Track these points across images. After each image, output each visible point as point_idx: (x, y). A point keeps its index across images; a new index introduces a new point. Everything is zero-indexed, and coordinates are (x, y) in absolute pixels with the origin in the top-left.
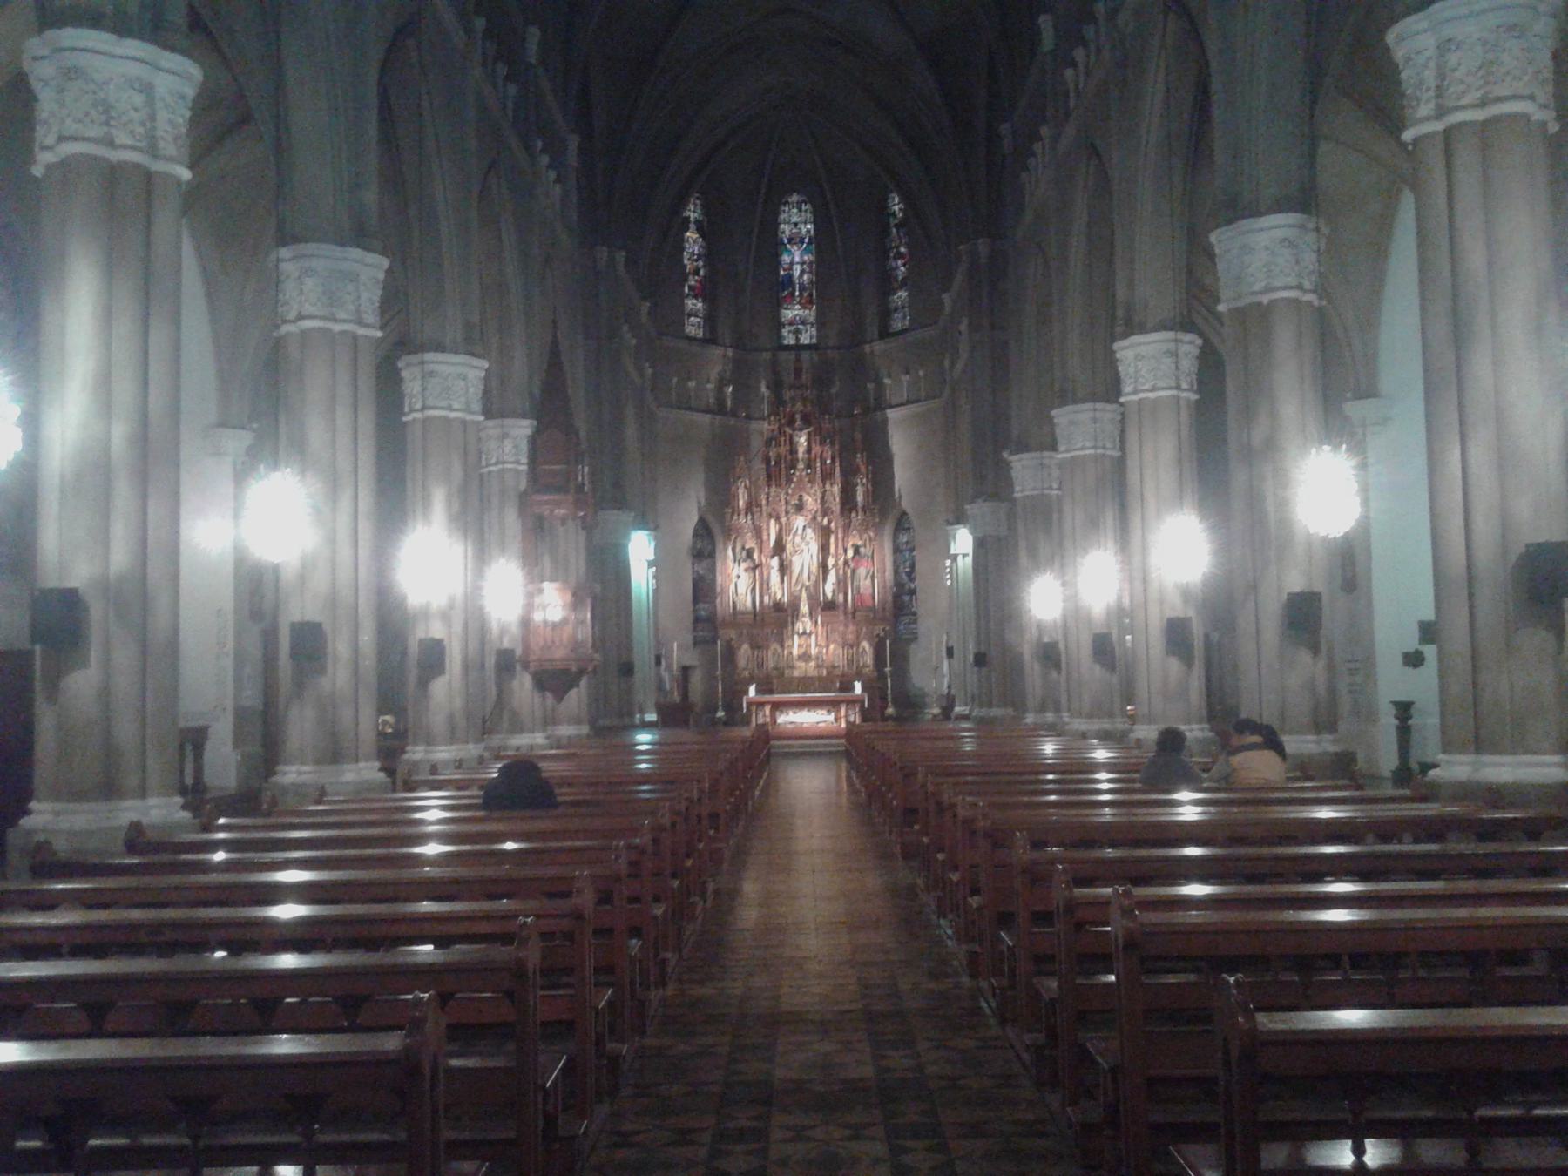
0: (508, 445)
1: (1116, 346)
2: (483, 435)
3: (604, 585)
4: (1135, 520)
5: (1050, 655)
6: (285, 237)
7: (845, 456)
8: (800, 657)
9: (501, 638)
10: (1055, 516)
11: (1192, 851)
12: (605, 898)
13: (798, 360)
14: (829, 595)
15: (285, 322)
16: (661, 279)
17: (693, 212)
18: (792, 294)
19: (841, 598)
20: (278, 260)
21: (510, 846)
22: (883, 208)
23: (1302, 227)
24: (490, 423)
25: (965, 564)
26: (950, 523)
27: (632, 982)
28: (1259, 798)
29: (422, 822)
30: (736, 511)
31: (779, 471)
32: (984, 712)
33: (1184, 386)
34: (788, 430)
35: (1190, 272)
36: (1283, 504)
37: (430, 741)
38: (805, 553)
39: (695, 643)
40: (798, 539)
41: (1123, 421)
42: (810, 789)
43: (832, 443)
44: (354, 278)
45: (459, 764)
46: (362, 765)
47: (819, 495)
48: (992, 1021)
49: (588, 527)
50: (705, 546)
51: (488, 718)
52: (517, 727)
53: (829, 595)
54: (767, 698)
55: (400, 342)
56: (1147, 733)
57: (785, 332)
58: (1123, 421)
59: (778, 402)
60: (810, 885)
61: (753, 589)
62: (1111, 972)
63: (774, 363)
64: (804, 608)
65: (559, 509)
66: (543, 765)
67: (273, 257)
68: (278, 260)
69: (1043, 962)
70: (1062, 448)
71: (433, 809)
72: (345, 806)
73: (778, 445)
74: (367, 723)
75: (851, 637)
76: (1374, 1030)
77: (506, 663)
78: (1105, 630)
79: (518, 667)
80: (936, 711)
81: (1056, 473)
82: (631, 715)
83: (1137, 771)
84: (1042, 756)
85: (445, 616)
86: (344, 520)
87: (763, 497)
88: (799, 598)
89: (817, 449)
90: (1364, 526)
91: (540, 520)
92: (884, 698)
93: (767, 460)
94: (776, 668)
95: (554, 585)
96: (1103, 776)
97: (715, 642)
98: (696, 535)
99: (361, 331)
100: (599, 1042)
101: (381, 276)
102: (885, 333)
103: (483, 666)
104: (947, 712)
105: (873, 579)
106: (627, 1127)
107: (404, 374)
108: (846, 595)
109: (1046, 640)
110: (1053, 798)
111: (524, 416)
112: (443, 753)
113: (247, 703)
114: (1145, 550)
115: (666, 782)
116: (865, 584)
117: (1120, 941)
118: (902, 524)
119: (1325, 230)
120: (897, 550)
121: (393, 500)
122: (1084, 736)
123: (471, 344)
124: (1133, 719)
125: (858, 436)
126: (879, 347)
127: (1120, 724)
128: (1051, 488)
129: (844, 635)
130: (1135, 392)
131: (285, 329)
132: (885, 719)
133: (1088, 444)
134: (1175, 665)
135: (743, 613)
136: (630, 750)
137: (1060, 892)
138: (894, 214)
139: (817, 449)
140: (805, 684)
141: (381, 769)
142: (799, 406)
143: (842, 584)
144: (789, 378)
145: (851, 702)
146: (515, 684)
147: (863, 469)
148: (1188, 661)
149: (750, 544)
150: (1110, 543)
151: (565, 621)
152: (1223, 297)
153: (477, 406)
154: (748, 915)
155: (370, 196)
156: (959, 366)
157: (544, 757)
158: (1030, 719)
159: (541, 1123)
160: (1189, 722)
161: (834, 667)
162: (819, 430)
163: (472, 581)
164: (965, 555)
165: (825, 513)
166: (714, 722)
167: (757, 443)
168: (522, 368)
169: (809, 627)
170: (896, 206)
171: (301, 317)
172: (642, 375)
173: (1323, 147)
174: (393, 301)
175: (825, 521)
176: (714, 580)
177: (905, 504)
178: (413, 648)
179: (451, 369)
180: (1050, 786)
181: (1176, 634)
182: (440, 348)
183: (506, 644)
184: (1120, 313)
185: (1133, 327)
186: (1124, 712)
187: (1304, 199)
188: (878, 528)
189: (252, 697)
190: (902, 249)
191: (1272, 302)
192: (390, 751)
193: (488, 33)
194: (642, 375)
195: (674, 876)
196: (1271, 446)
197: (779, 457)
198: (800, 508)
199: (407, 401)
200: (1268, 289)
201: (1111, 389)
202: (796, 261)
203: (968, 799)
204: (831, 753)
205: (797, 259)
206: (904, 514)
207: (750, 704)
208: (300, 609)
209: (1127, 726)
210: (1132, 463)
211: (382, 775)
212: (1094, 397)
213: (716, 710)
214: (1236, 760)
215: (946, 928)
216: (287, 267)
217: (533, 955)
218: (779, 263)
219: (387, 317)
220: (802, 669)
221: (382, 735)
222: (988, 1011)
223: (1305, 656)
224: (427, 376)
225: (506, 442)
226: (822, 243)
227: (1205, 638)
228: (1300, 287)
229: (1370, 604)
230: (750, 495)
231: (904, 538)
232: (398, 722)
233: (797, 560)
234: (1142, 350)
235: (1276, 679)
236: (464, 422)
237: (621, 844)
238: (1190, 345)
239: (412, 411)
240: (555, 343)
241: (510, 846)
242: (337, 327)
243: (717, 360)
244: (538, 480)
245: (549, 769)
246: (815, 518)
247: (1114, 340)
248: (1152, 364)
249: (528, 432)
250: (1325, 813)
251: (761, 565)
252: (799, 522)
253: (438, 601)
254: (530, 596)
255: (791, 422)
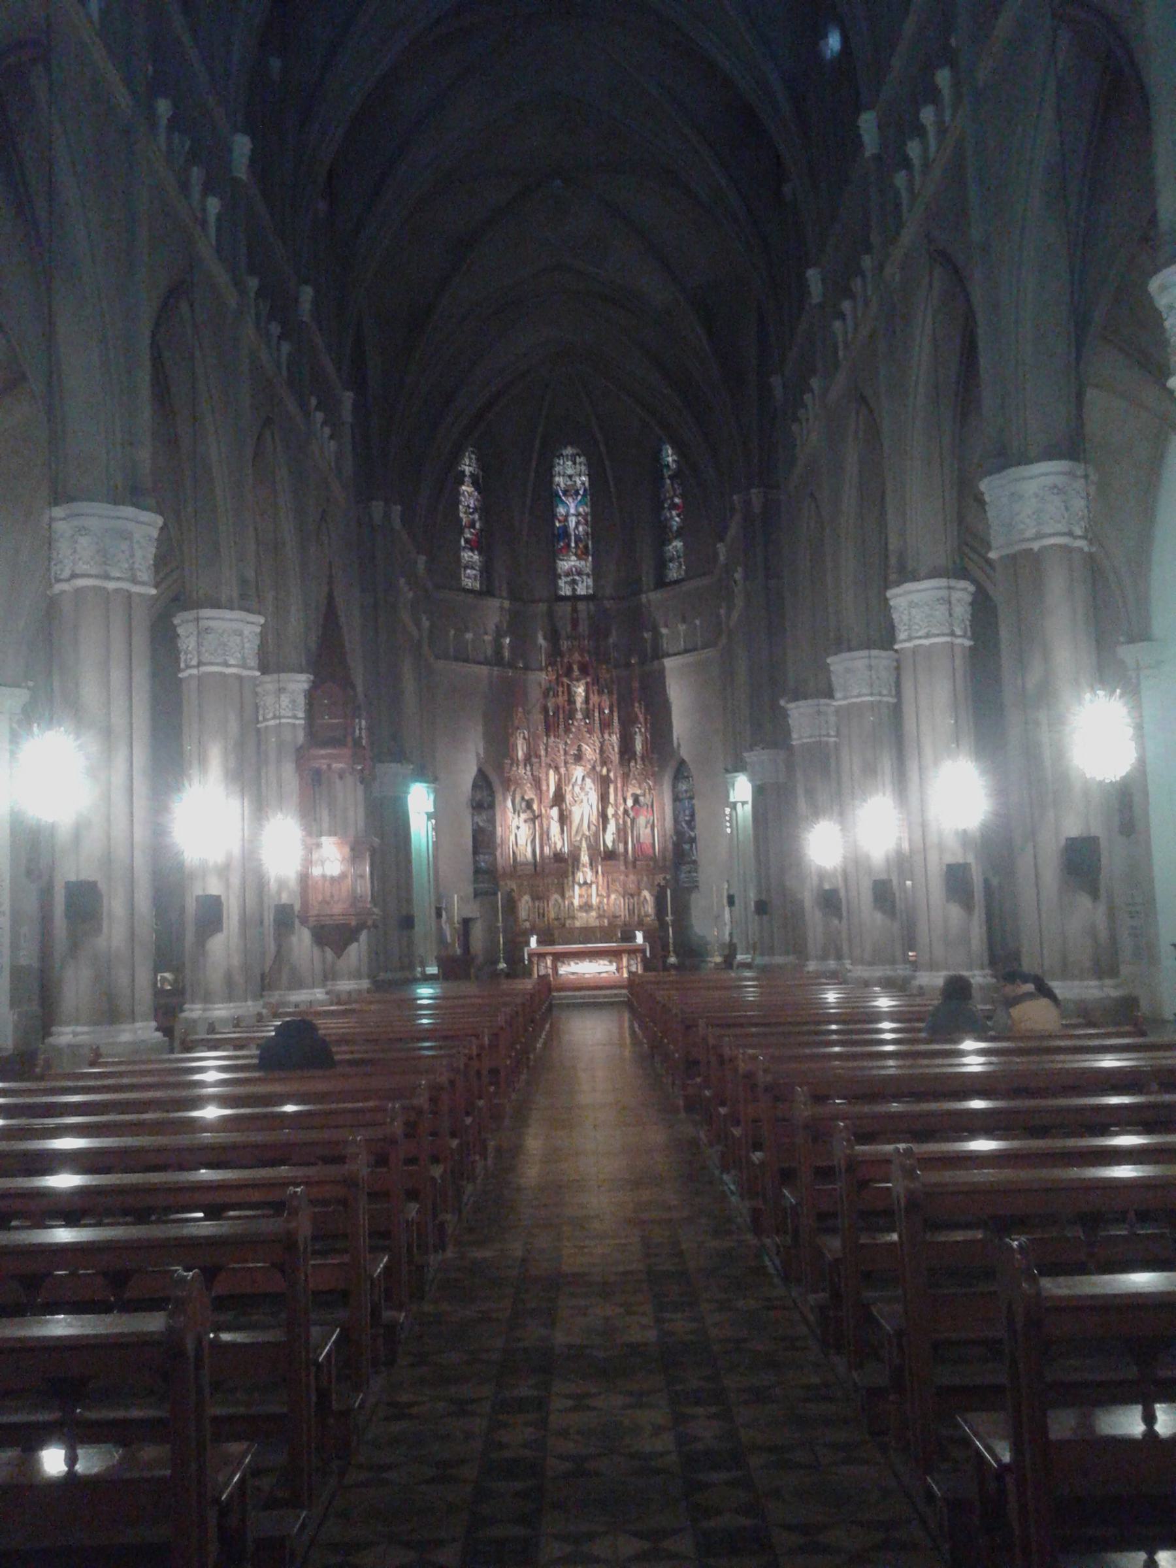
0: (285, 700)
1: (889, 594)
2: (259, 689)
3: (384, 840)
4: (913, 775)
5: (830, 901)
6: (59, 496)
7: (623, 704)
8: (581, 907)
9: (279, 893)
10: (833, 762)
11: (977, 1104)
12: (381, 1160)
13: (575, 610)
14: (610, 845)
15: (58, 581)
16: (438, 530)
17: (468, 466)
18: (568, 545)
19: (621, 847)
20: (51, 519)
21: (290, 1108)
22: (657, 456)
23: (1071, 474)
24: (267, 678)
25: (745, 812)
26: (727, 771)
27: (410, 1247)
28: (1039, 1046)
29: (202, 1084)
30: (515, 762)
31: (557, 721)
32: (766, 960)
33: (959, 632)
34: (565, 680)
35: (961, 519)
36: (1060, 755)
37: (207, 998)
38: (584, 803)
39: (476, 895)
40: (577, 789)
41: (898, 668)
42: (593, 1038)
43: (610, 693)
44: (127, 536)
45: (237, 1022)
46: (138, 1025)
47: (598, 744)
48: (776, 1280)
49: (366, 780)
50: (484, 799)
51: (265, 978)
52: (297, 983)
53: (610, 845)
54: (550, 949)
55: (177, 594)
56: (934, 980)
57: (561, 583)
58: (898, 668)
59: (555, 652)
60: (595, 1136)
61: (533, 840)
62: (894, 1231)
63: (550, 614)
64: (585, 858)
65: (335, 761)
66: (318, 1022)
67: (46, 519)
68: (51, 519)
69: (825, 1220)
70: (838, 695)
71: (211, 1069)
72: (123, 1068)
73: (556, 695)
74: (140, 981)
75: (632, 886)
76: (1162, 1294)
77: (285, 919)
78: (884, 876)
79: (297, 922)
80: (718, 959)
81: (833, 719)
82: (411, 967)
83: (919, 1020)
84: (825, 1005)
85: (224, 871)
86: (118, 779)
87: (542, 747)
88: (579, 849)
89: (594, 699)
90: (1142, 762)
91: (318, 773)
92: (665, 947)
93: (545, 710)
94: (557, 919)
95: (333, 839)
96: (886, 1025)
97: (495, 894)
98: (475, 786)
99: (136, 589)
100: (375, 1313)
101: (155, 534)
102: (661, 583)
103: (262, 923)
104: (729, 962)
105: (653, 828)
106: (404, 1398)
107: (180, 631)
108: (626, 844)
109: (827, 887)
110: (837, 1049)
111: (301, 671)
112: (221, 1011)
113: (24, 962)
114: (922, 802)
115: (446, 1038)
116: (644, 833)
117: (903, 1201)
118: (681, 772)
119: (1094, 477)
120: (676, 799)
121: (168, 760)
122: (867, 984)
123: (246, 601)
124: (915, 966)
125: (636, 685)
126: (655, 596)
127: (901, 971)
128: (828, 735)
129: (624, 885)
130: (910, 639)
131: (58, 587)
132: (666, 968)
133: (865, 691)
134: (955, 911)
135: (523, 864)
136: (411, 1003)
137: (841, 1149)
138: (668, 466)
139: (594, 699)
140: (587, 934)
141: (157, 1029)
142: (576, 656)
143: (622, 833)
144: (565, 628)
145: (631, 952)
146: (294, 939)
147: (641, 718)
148: (968, 907)
149: (530, 795)
150: (889, 788)
151: (343, 876)
152: (994, 544)
153: (253, 662)
154: (531, 1173)
155: (144, 454)
156: (735, 615)
157: (318, 1014)
158: (812, 966)
159: (314, 1399)
160: (970, 968)
161: (615, 917)
162: (596, 681)
163: (248, 837)
164: (744, 803)
165: (604, 763)
166: (496, 975)
167: (535, 694)
168: (298, 624)
169: (590, 876)
170: (670, 457)
171: (74, 576)
172: (418, 624)
173: (1091, 394)
174: (167, 559)
175: (604, 771)
176: (493, 833)
177: (684, 753)
178: (191, 906)
179: (227, 625)
180: (835, 1037)
181: (957, 880)
182: (217, 605)
183: (285, 898)
184: (893, 561)
185: (907, 575)
186: (906, 960)
187: (1072, 446)
188: (657, 777)
189: (28, 957)
190: (677, 500)
191: (1044, 549)
192: (167, 1010)
193: (259, 293)
194: (418, 624)
195: (453, 1135)
196: (1045, 695)
197: (557, 709)
198: (579, 758)
199: (183, 657)
200: (1039, 536)
201: (885, 637)
202: (572, 512)
203: (750, 1051)
204: (612, 1004)
205: (572, 511)
206: (682, 762)
207: (530, 956)
208: (70, 871)
209: (908, 973)
210: (908, 709)
211: (159, 1034)
212: (869, 645)
213: (497, 962)
214: (1015, 1012)
215: (729, 1181)
216: (61, 527)
217: (303, 1226)
218: (554, 516)
219: (162, 575)
220: (585, 919)
221: (158, 993)
222: (772, 1271)
223: (1084, 901)
224: (202, 632)
225: (283, 697)
226: (597, 494)
227: (987, 881)
228: (1070, 534)
229: (1148, 842)
230: (529, 747)
231: (683, 787)
232: (176, 981)
233: (576, 809)
234: (915, 597)
235: (1056, 922)
236: (239, 678)
237: (404, 1089)
238: (963, 591)
239: (188, 667)
240: (330, 597)
241: (290, 1108)
242: (111, 585)
243: (494, 611)
244: (316, 736)
245: (328, 1027)
246: (594, 768)
247: (886, 588)
248: (925, 610)
249: (306, 686)
250: (1109, 1062)
251: (540, 816)
252: (578, 772)
253: (216, 857)
254: (309, 850)
255: (569, 672)
